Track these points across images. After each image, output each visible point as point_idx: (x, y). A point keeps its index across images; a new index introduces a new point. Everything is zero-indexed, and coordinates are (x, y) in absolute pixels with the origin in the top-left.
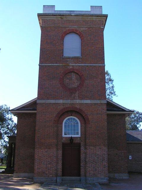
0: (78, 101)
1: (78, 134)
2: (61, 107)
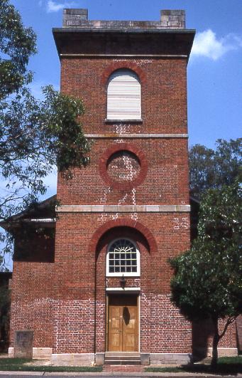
0: (136, 207)
1: (135, 270)
2: (103, 219)
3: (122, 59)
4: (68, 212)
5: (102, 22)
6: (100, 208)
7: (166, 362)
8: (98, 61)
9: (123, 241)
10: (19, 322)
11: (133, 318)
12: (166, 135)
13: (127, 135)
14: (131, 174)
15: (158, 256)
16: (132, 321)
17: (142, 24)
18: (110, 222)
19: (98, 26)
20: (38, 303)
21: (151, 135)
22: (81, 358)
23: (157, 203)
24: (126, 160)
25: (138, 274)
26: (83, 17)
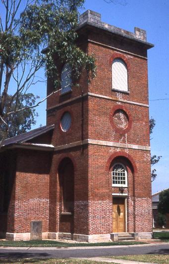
1: (124, 183)
2: (112, 151)
3: (119, 52)
4: (95, 144)
5: (109, 25)
6: (111, 144)
7: (51, 237)
8: (107, 50)
9: (119, 165)
10: (20, 215)
11: (122, 212)
12: (140, 104)
13: (122, 100)
14: (124, 125)
15: (138, 175)
16: (122, 214)
17: (128, 33)
18: (116, 153)
19: (106, 26)
20: (32, 201)
21: (133, 103)
22: (104, 237)
23: (137, 144)
24: (122, 115)
25: (126, 185)
26: (99, 19)
